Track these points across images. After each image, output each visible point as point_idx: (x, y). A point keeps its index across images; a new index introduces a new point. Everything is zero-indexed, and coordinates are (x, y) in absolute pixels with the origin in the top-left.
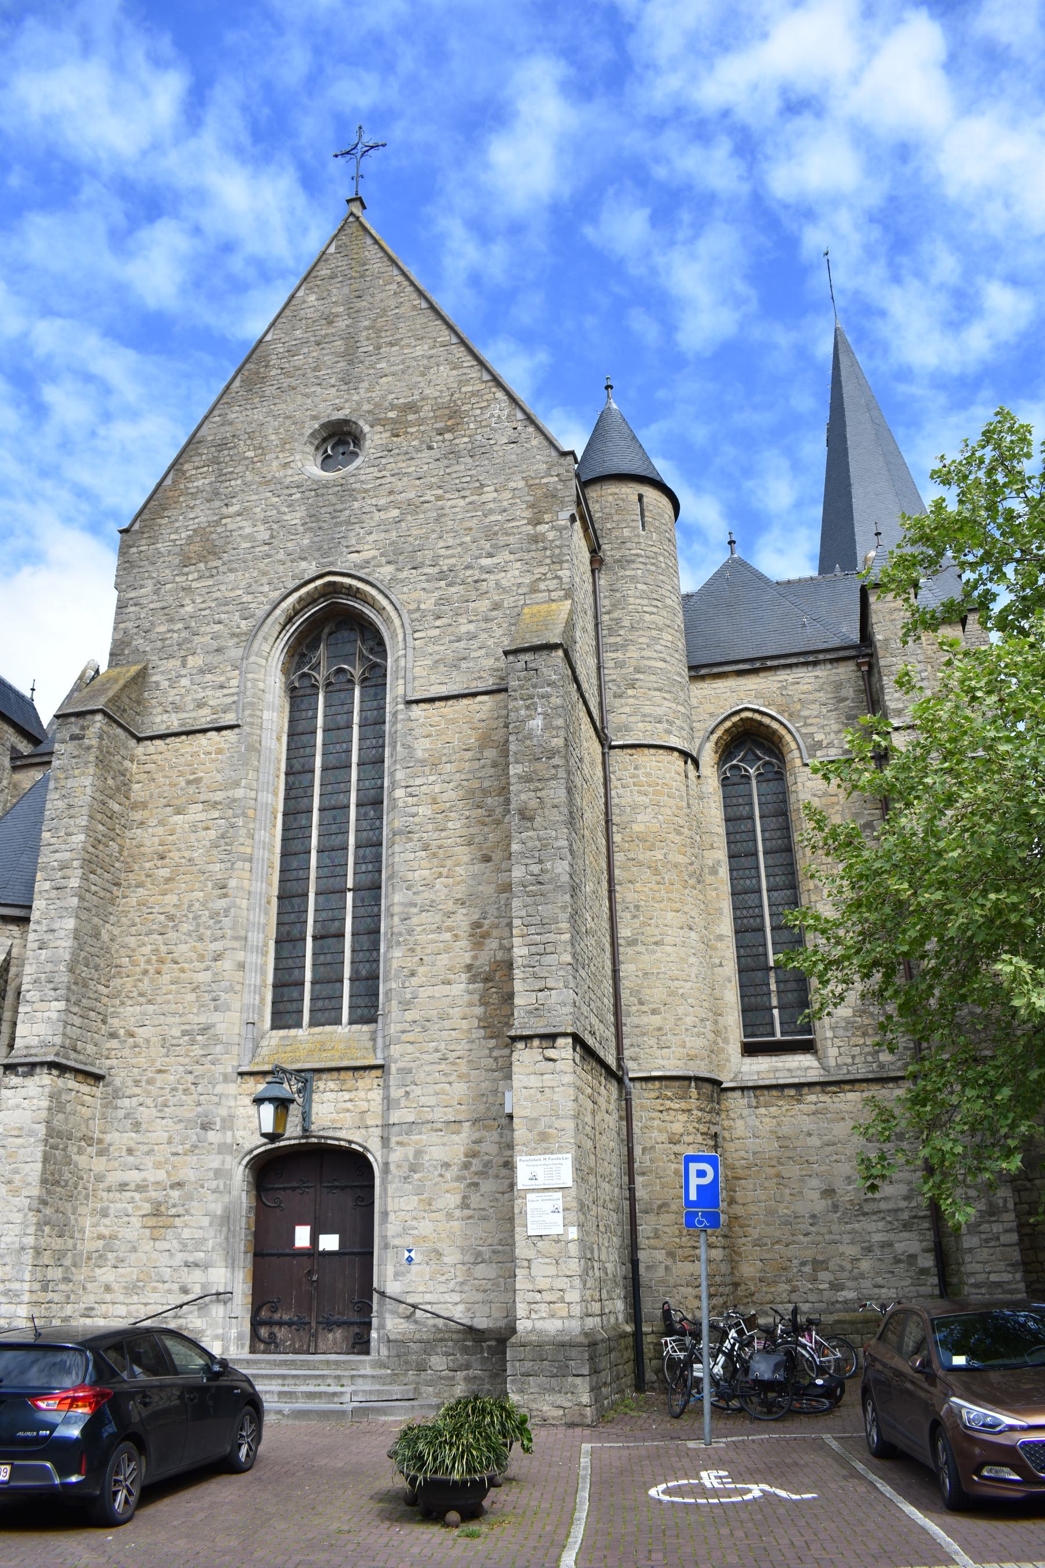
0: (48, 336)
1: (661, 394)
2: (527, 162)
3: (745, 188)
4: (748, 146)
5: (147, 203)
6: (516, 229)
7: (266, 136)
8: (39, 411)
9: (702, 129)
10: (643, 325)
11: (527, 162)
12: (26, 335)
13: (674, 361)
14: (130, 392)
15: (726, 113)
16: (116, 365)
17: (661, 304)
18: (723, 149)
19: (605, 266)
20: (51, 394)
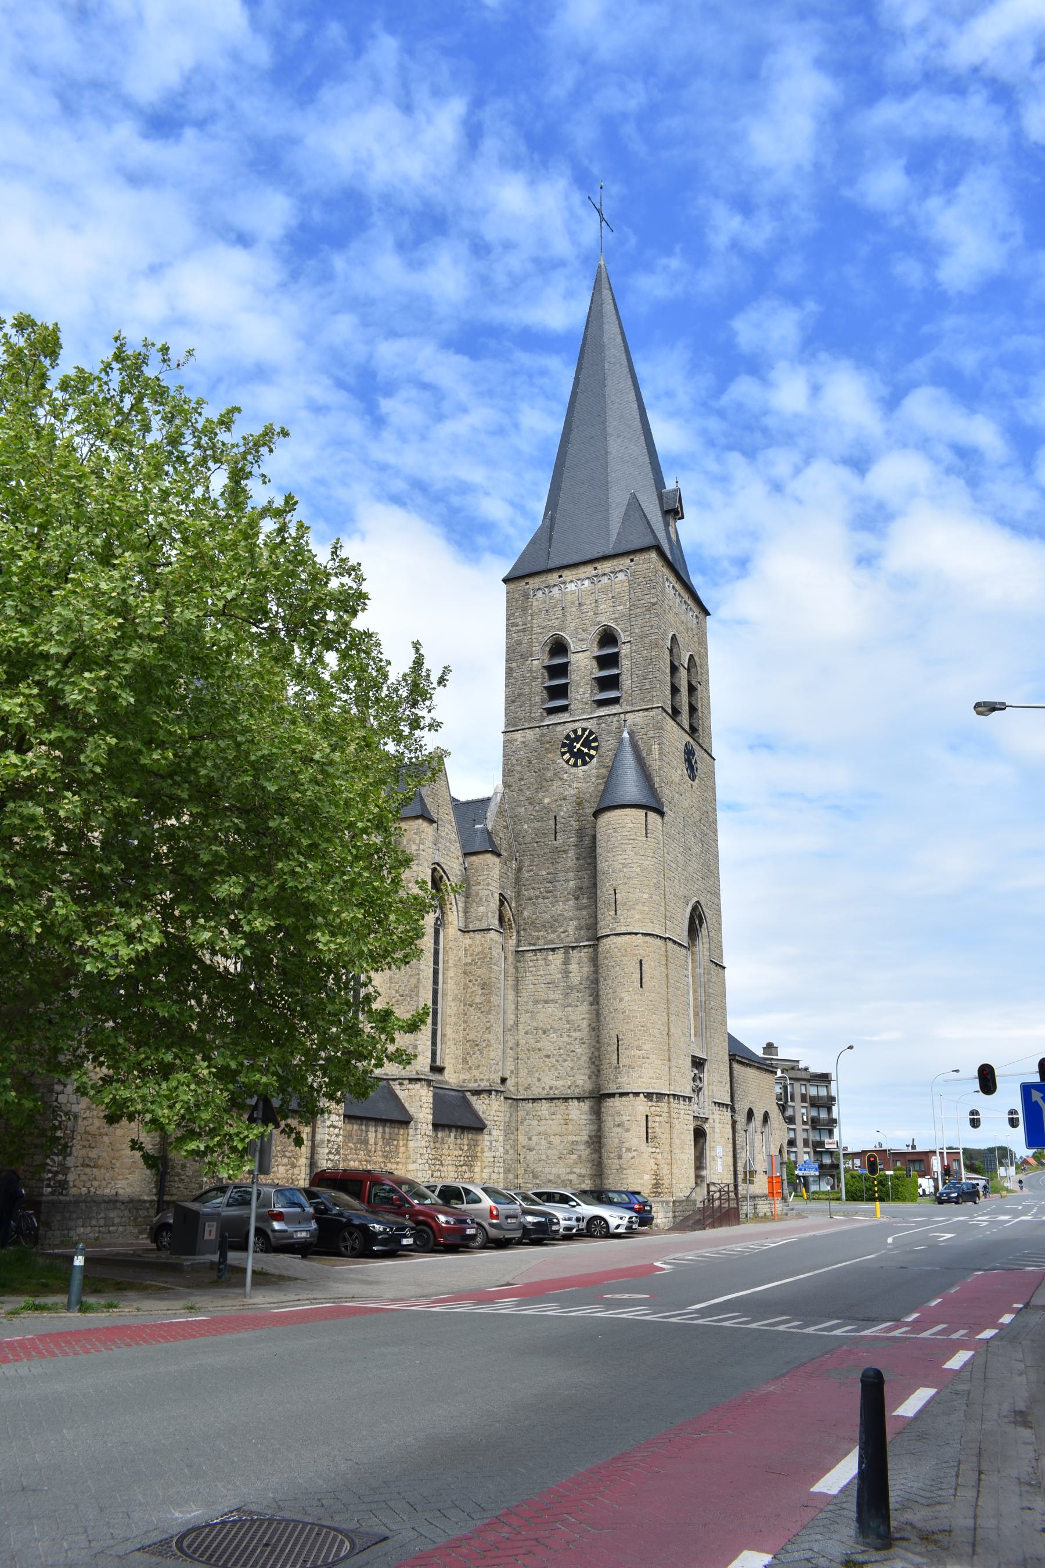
0: (388, 353)
1: (926, 329)
2: (785, 129)
3: (1004, 133)
4: (1004, 95)
5: (427, 224)
6: (779, 204)
7: (540, 147)
8: (378, 422)
9: (957, 85)
10: (908, 271)
11: (785, 129)
12: (371, 357)
13: (936, 300)
14: (462, 392)
15: (975, 70)
16: (448, 370)
17: (929, 252)
18: (977, 100)
19: (868, 220)
20: (386, 405)
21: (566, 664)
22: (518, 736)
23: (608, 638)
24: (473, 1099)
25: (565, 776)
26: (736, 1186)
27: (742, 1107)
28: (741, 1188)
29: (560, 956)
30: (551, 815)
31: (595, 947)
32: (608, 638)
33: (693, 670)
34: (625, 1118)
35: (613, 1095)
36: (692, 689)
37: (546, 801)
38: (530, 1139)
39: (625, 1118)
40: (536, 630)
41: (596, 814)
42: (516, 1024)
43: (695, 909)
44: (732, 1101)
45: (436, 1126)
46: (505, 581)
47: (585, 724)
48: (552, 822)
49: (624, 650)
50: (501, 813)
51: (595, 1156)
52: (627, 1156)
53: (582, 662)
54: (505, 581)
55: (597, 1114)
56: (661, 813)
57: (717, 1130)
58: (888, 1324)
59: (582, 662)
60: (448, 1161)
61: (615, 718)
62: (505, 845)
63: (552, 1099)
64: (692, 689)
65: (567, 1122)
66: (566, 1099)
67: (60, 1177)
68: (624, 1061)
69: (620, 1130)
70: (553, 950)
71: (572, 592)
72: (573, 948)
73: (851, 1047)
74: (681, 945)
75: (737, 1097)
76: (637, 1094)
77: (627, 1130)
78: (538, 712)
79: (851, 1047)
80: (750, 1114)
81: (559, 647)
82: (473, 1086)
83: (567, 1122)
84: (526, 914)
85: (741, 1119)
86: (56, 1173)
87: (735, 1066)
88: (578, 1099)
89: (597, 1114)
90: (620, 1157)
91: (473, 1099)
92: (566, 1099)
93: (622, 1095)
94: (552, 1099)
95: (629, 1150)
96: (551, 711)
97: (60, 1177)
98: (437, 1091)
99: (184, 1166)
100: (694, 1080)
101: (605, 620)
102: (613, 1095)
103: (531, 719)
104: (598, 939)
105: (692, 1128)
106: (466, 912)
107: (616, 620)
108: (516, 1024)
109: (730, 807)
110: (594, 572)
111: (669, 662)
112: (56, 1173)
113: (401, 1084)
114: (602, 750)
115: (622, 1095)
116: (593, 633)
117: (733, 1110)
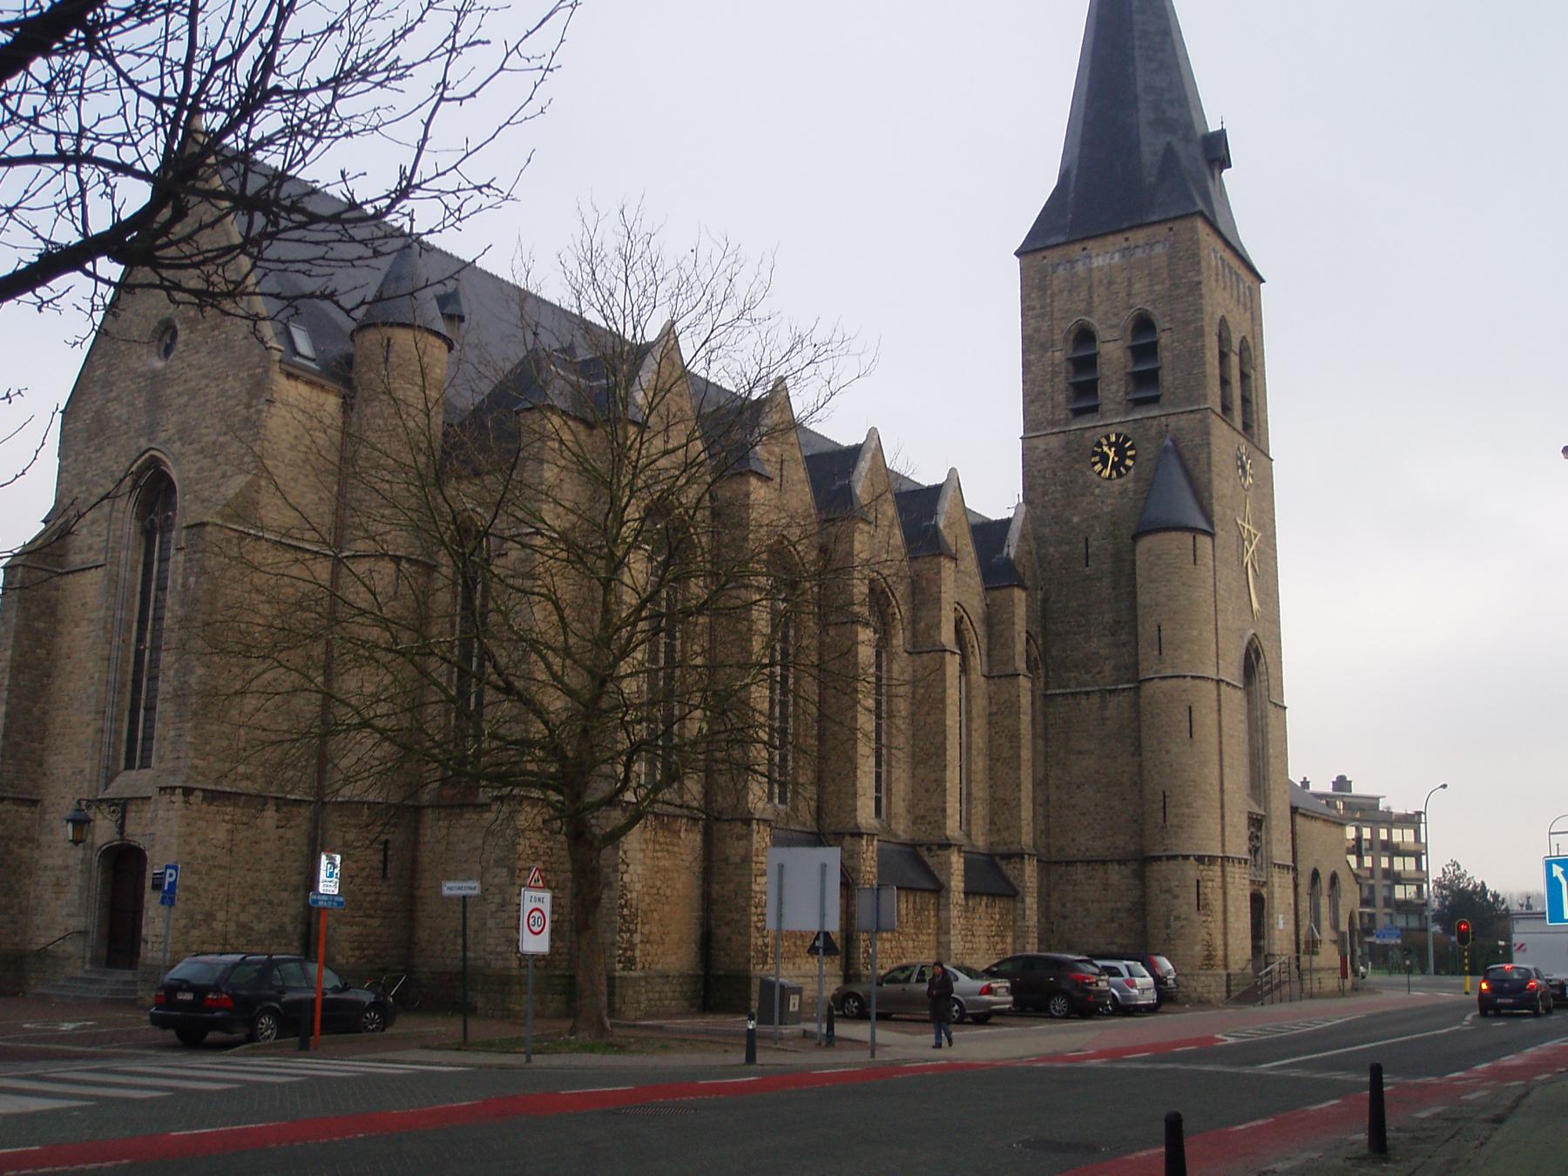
21: (1095, 355)
22: (1036, 442)
23: (1144, 324)
24: (1003, 864)
25: (1097, 491)
26: (1298, 959)
27: (1305, 868)
28: (1304, 959)
29: (1095, 699)
30: (1081, 537)
31: (1137, 689)
32: (1144, 324)
33: (1246, 354)
34: (1173, 884)
35: (1159, 858)
36: (1244, 377)
37: (1076, 519)
38: (1064, 905)
39: (1173, 884)
40: (1058, 315)
41: (1136, 537)
42: (1046, 777)
43: (1250, 643)
44: (1294, 861)
45: (966, 894)
46: (1017, 254)
47: (1120, 429)
48: (1082, 545)
49: (1164, 339)
50: (1023, 537)
51: (943, 938)
52: (1175, 925)
53: (1113, 351)
54: (1017, 254)
55: (1140, 876)
56: (1212, 535)
57: (1277, 895)
58: (1471, 1097)
59: (1113, 351)
60: (980, 931)
61: (1155, 422)
62: (1028, 574)
63: (1089, 862)
64: (1244, 377)
65: (1106, 887)
66: (1104, 862)
67: (629, 953)
68: (1171, 820)
69: (1168, 896)
70: (1087, 693)
71: (1100, 269)
72: (1111, 692)
73: (1444, 786)
74: (1235, 687)
75: (1299, 857)
76: (1186, 857)
77: (1176, 897)
78: (1062, 414)
79: (1444, 786)
80: (1315, 875)
81: (1085, 336)
82: (1003, 849)
83: (1106, 887)
84: (1054, 653)
85: (1304, 882)
86: (625, 950)
87: (1299, 819)
88: (1119, 862)
89: (1140, 876)
90: (1168, 926)
91: (1003, 864)
92: (1104, 862)
93: (1169, 858)
94: (1089, 862)
95: (1177, 918)
96: (1078, 413)
97: (629, 953)
98: (886, 846)
99: (729, 939)
100: (1250, 839)
101: (1139, 303)
102: (1159, 858)
103: (1054, 423)
104: (1140, 682)
105: (1248, 893)
106: (989, 656)
107: (1154, 302)
108: (1046, 777)
109: (1334, 969)
110: (1125, 244)
111: (1217, 351)
112: (625, 950)
113: (929, 850)
114: (1139, 460)
115: (1169, 858)
116: (1126, 317)
117: (1295, 869)
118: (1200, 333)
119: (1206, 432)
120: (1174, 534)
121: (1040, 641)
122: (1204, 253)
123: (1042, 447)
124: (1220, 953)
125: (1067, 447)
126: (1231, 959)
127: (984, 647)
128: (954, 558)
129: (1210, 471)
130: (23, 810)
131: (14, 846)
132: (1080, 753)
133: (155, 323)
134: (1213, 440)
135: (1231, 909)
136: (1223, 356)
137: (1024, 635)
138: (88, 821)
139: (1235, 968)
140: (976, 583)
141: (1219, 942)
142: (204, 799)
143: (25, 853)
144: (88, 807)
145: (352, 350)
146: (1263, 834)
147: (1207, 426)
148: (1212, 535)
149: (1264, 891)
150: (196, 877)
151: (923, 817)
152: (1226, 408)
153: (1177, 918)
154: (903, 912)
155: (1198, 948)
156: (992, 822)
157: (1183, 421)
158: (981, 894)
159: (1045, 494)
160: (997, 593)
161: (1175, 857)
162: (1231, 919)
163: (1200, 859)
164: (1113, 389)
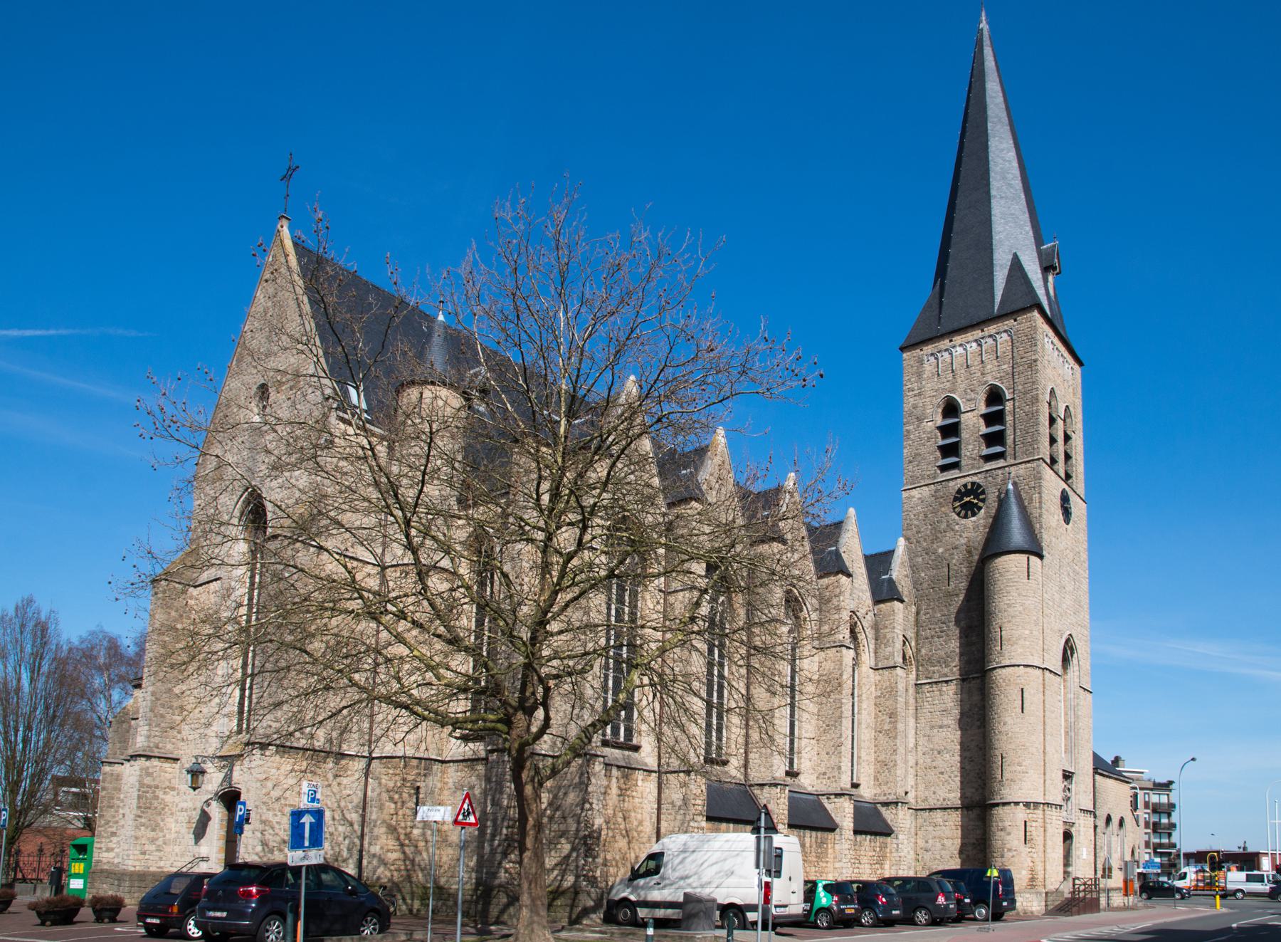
27: (1102, 814)
32: (995, 396)
34: (1007, 824)
37: (941, 550)
43: (1067, 641)
53: (972, 422)
59: (972, 422)
60: (864, 860)
70: (946, 682)
76: (1017, 803)
77: (1009, 834)
81: (951, 408)
82: (883, 799)
90: (1002, 856)
91: (883, 810)
95: (1010, 850)
96: (944, 468)
106: (876, 653)
107: (1001, 379)
115: (1005, 804)
118: (1035, 400)
119: (1038, 477)
120: (1012, 556)
121: (913, 644)
122: (1039, 337)
123: (918, 496)
124: (1040, 877)
125: (935, 496)
126: (1047, 882)
127: (872, 646)
128: (849, 575)
129: (1041, 508)
130: (167, 765)
131: (160, 793)
132: (941, 727)
133: (254, 389)
134: (1044, 483)
135: (1049, 843)
136: (1052, 421)
137: (901, 638)
138: (203, 772)
139: (1051, 887)
140: (867, 598)
141: (1039, 868)
142: (277, 752)
143: (168, 798)
144: (204, 762)
145: (1028, 902)
146: (1073, 787)
147: (1039, 473)
148: (1041, 557)
149: (1073, 830)
150: (271, 813)
151: (824, 774)
152: (1053, 461)
153: (1010, 850)
154: (808, 845)
155: (1024, 872)
156: (876, 779)
157: (1021, 470)
158: (866, 833)
159: (918, 532)
160: (882, 605)
161: (1009, 803)
162: (1048, 851)
163: (1027, 805)
164: (972, 447)
